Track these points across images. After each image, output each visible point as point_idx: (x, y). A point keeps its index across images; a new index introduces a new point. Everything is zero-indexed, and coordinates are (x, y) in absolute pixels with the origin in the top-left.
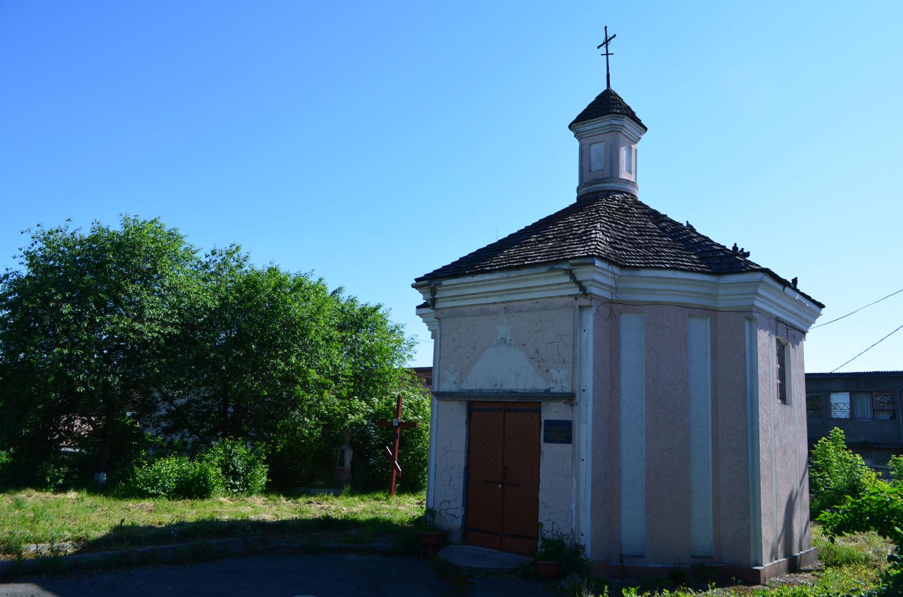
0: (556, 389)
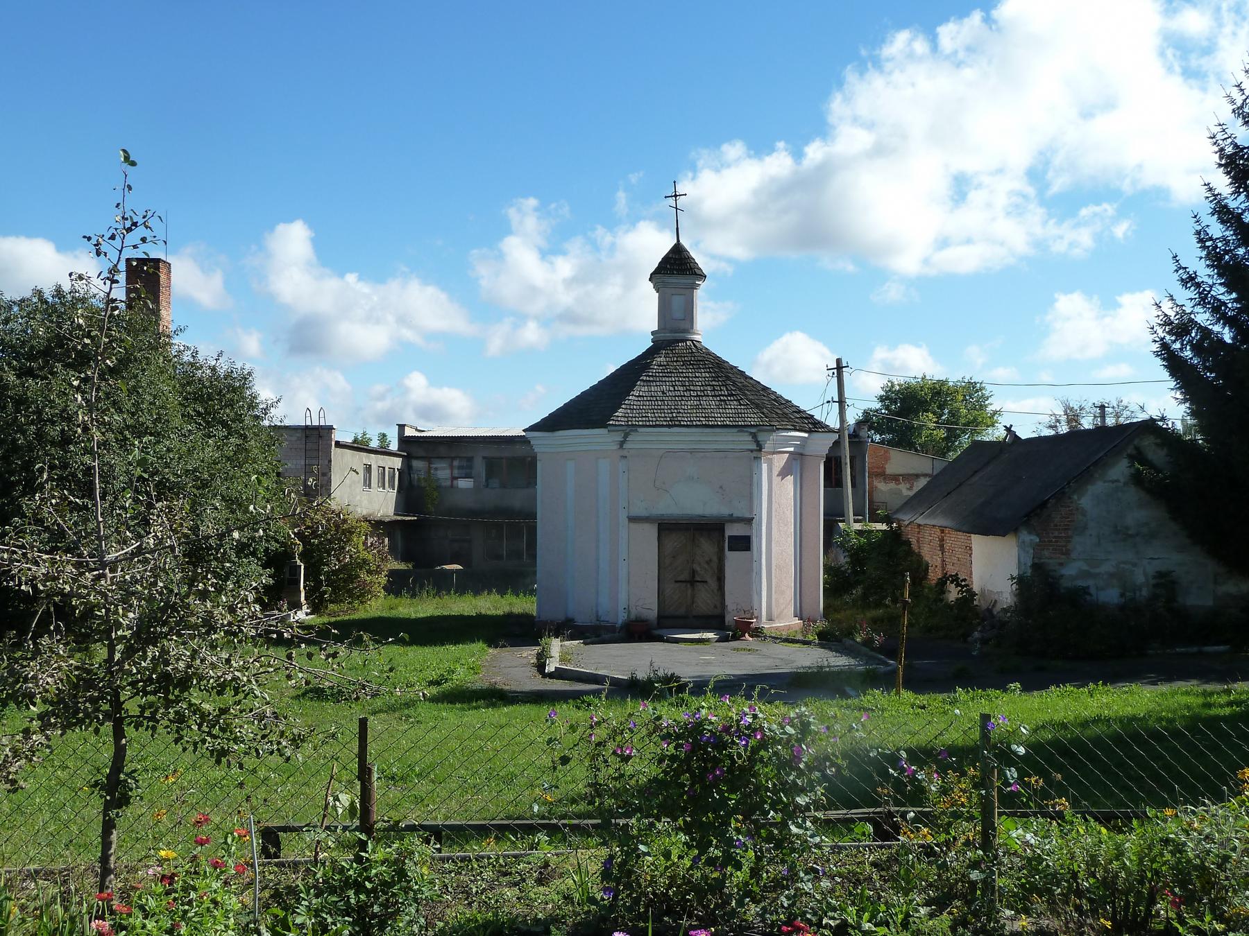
0: (737, 514)
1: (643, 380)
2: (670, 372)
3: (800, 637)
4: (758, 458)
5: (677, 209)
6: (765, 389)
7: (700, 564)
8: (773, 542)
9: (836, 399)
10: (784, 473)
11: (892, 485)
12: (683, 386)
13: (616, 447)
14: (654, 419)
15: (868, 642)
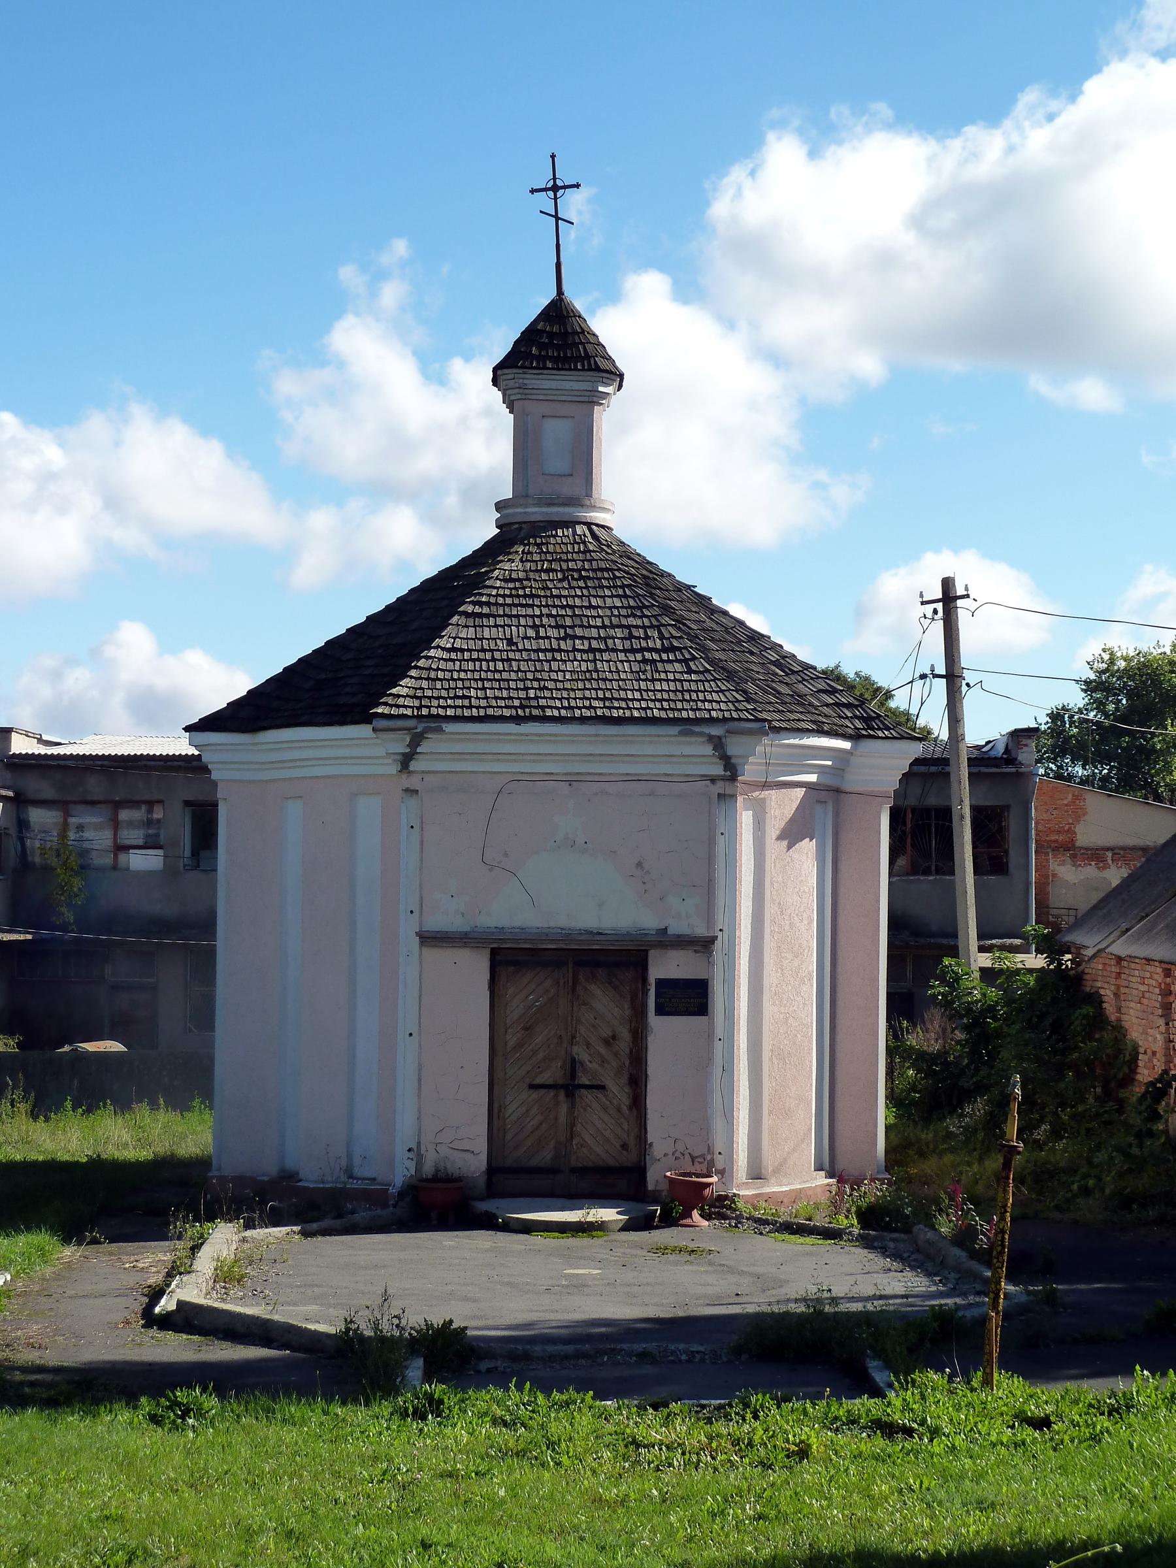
0: (677, 927)
1: (467, 615)
2: (532, 596)
3: (820, 1221)
4: (726, 798)
5: (557, 218)
6: (755, 637)
7: (588, 1045)
8: (766, 997)
9: (941, 669)
10: (793, 834)
11: (1090, 871)
12: (557, 627)
13: (393, 769)
14: (483, 703)
15: (965, 1237)
